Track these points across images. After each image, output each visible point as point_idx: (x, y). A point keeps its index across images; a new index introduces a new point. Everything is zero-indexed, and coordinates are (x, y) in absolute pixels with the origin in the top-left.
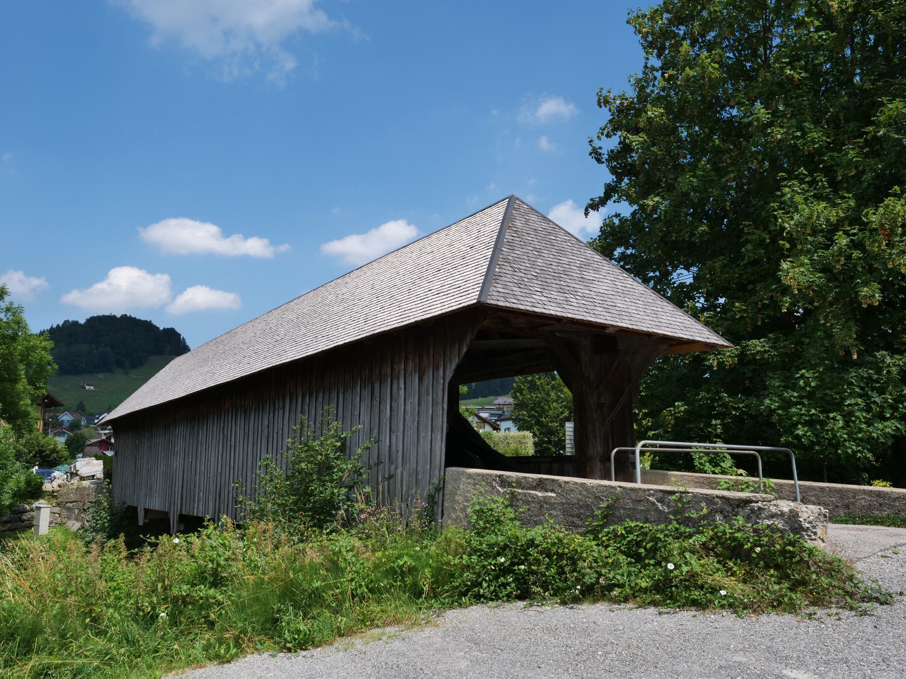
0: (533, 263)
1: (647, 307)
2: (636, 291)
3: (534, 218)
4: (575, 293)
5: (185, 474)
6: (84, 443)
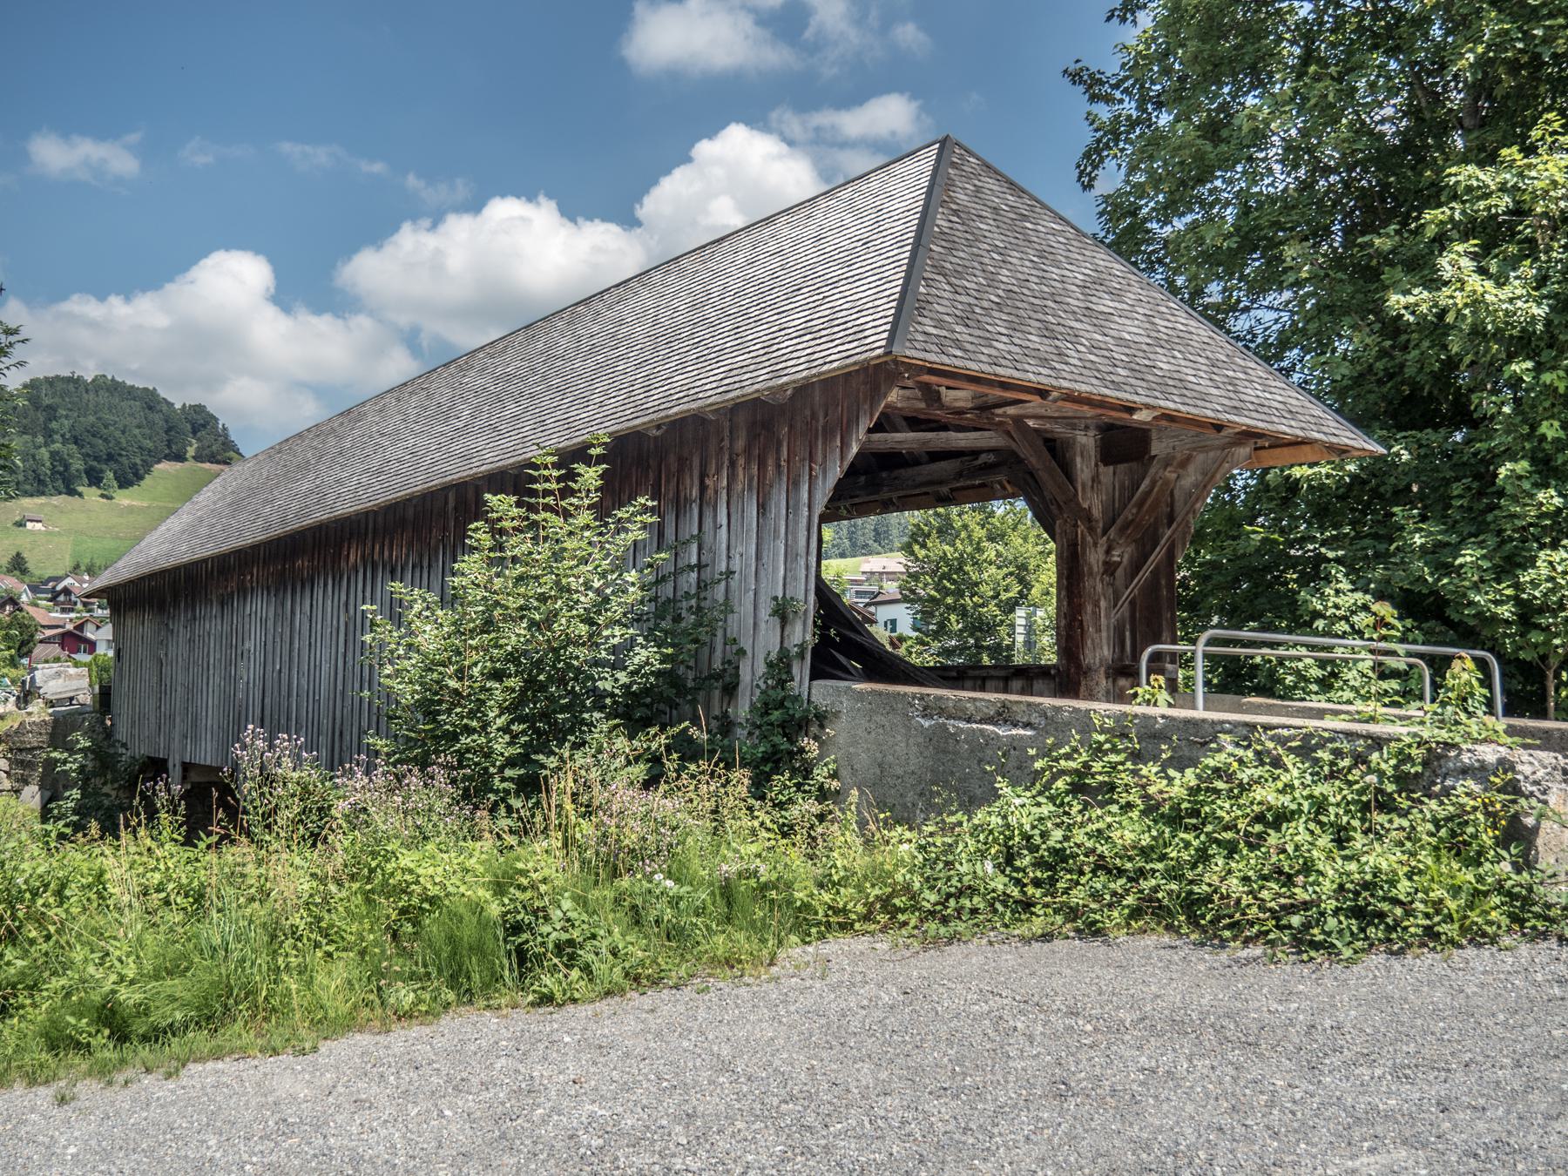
0: (991, 276)
1: (1215, 370)
2: (1195, 337)
3: (990, 183)
4: (1074, 339)
5: (268, 694)
6: (32, 636)
